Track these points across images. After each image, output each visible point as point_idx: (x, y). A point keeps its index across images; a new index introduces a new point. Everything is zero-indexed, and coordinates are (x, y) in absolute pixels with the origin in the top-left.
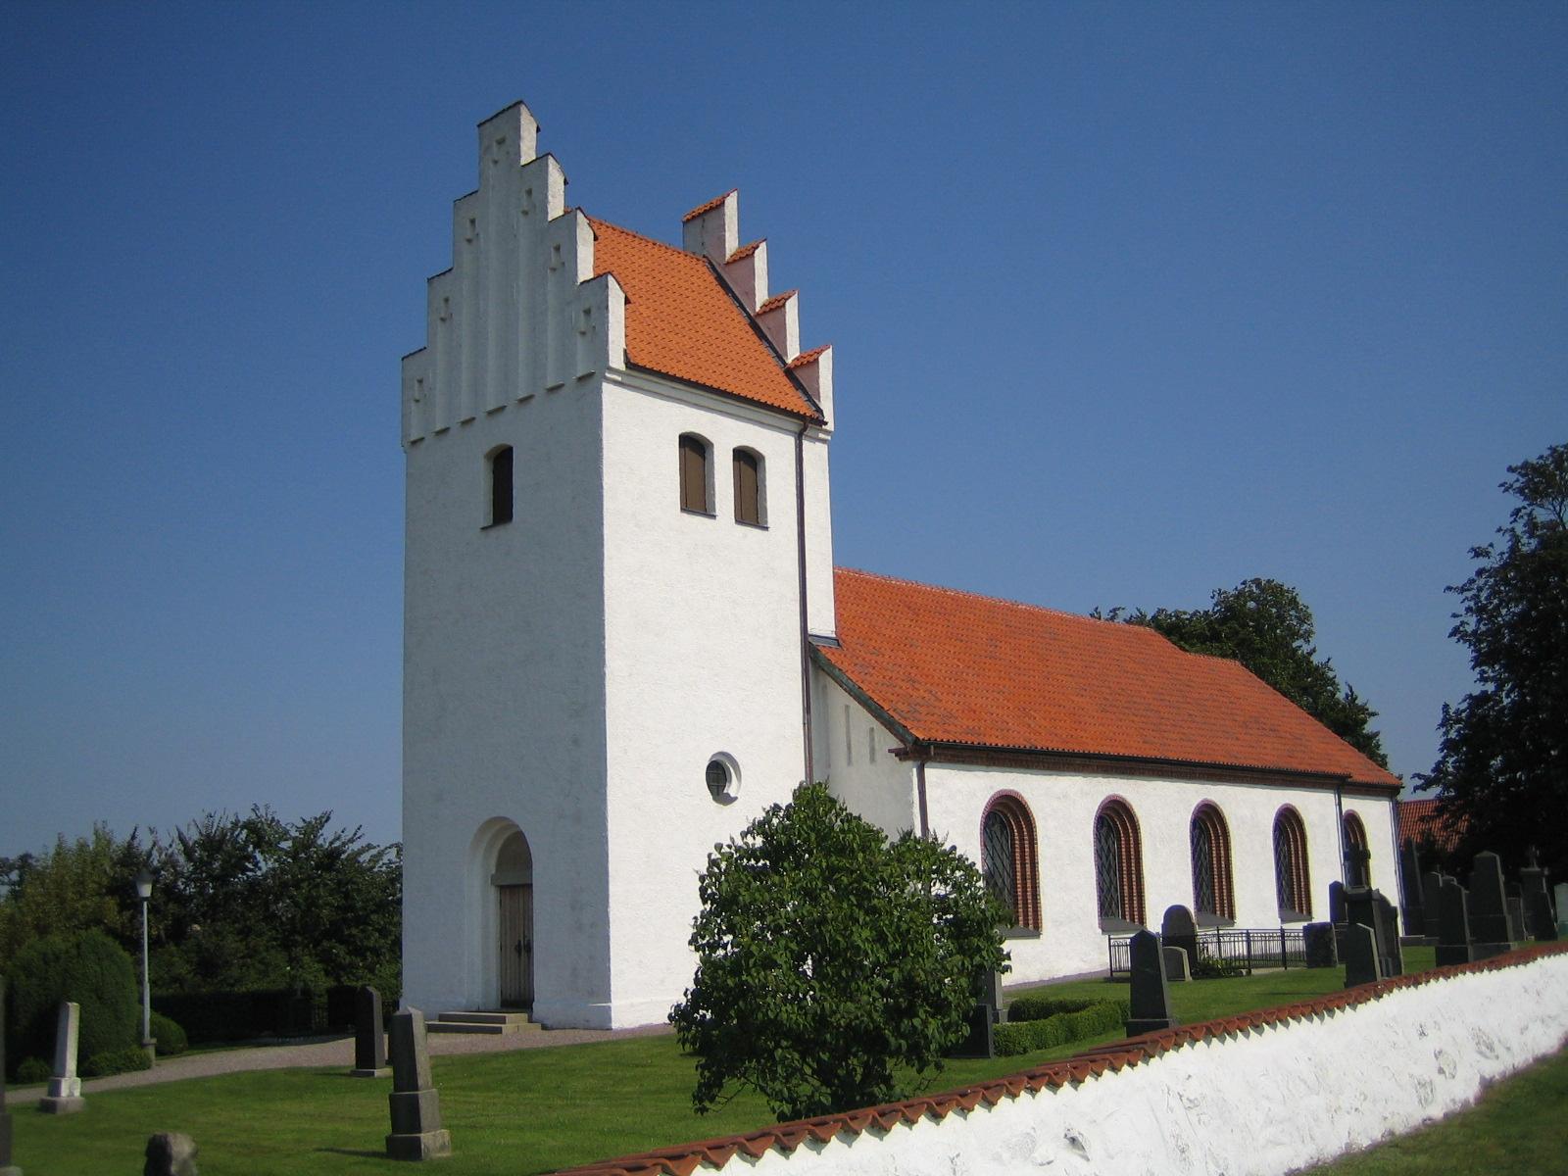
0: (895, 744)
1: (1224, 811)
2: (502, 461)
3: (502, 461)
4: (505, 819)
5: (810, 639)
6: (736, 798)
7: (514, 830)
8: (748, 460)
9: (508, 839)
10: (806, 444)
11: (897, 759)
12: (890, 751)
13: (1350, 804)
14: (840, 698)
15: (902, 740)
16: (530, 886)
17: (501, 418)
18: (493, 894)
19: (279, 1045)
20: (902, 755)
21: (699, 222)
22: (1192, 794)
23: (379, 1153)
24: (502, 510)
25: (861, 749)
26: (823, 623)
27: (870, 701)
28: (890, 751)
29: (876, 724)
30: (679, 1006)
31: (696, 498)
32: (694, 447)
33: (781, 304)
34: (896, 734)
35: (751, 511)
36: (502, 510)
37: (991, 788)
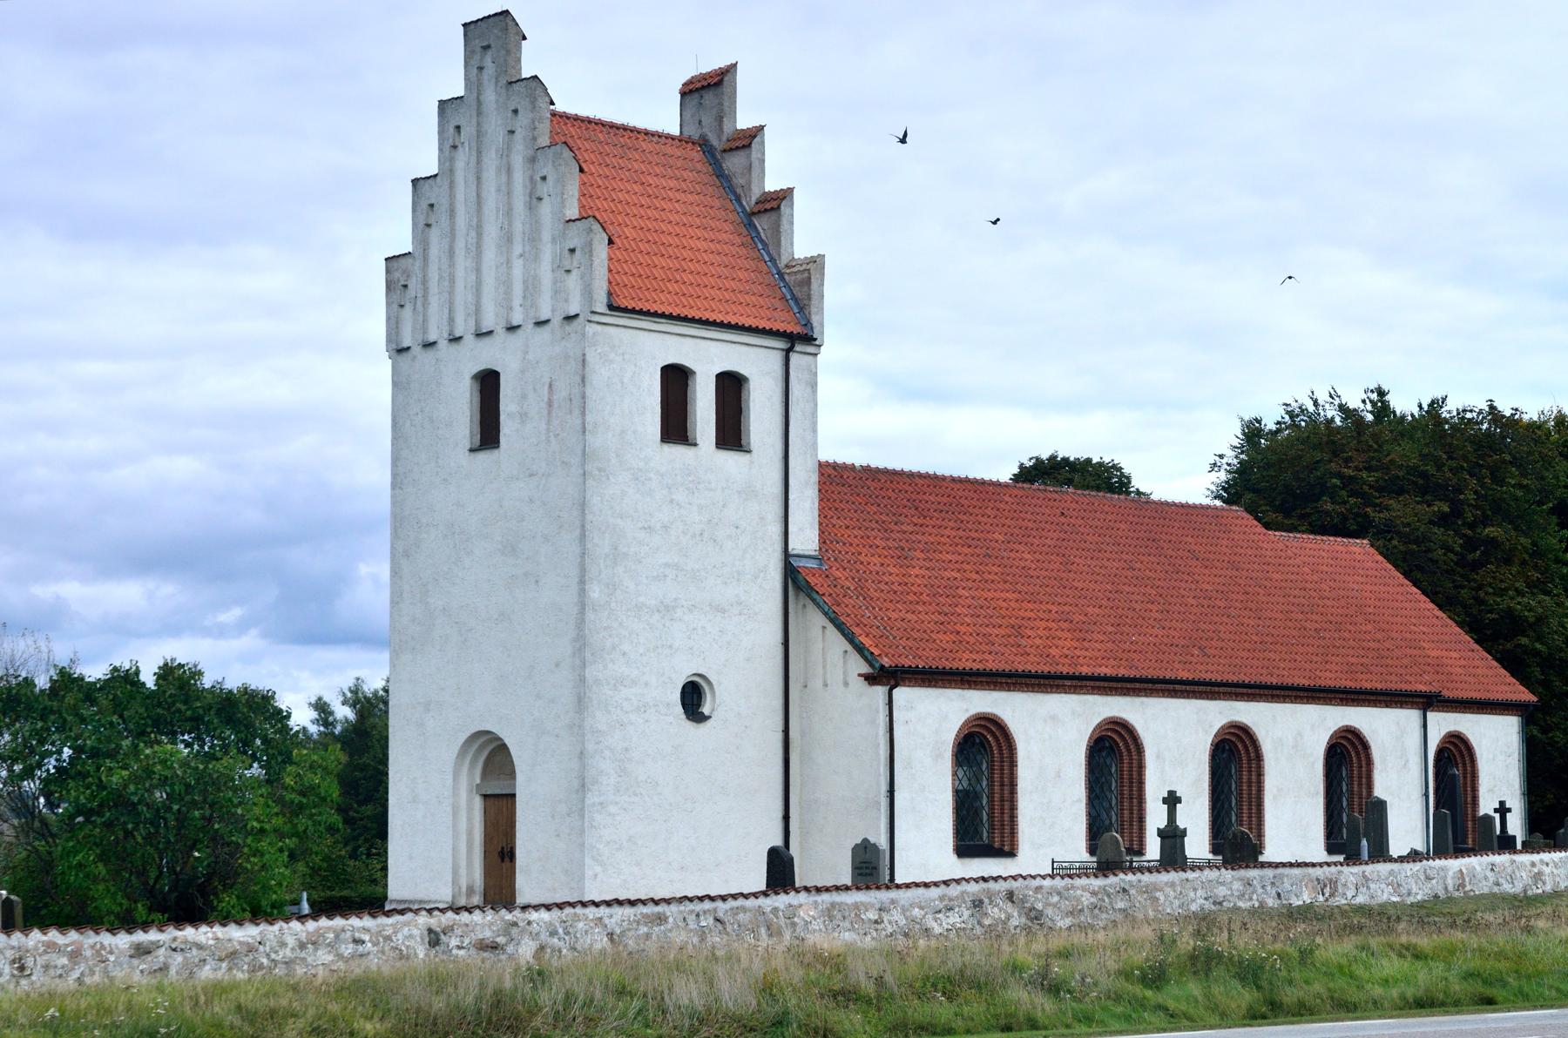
0: (865, 669)
1: (1257, 733)
2: (488, 382)
3: (488, 382)
4: (488, 732)
5: (795, 563)
6: (709, 717)
7: (499, 743)
8: (731, 387)
9: (493, 750)
10: (794, 358)
11: (866, 683)
12: (860, 675)
13: (1442, 723)
14: (817, 620)
15: (871, 665)
16: (514, 796)
17: (487, 341)
18: (478, 803)
19: (695, 415)
20: (871, 679)
21: (696, 95)
22: (1217, 714)
23: (477, 156)
24: (488, 434)
25: (836, 676)
26: (805, 539)
27: (844, 626)
28: (860, 675)
29: (849, 648)
30: (200, 673)
31: (675, 428)
32: (676, 380)
33: (774, 204)
34: (866, 659)
35: (731, 434)
36: (488, 434)
37: (967, 710)
